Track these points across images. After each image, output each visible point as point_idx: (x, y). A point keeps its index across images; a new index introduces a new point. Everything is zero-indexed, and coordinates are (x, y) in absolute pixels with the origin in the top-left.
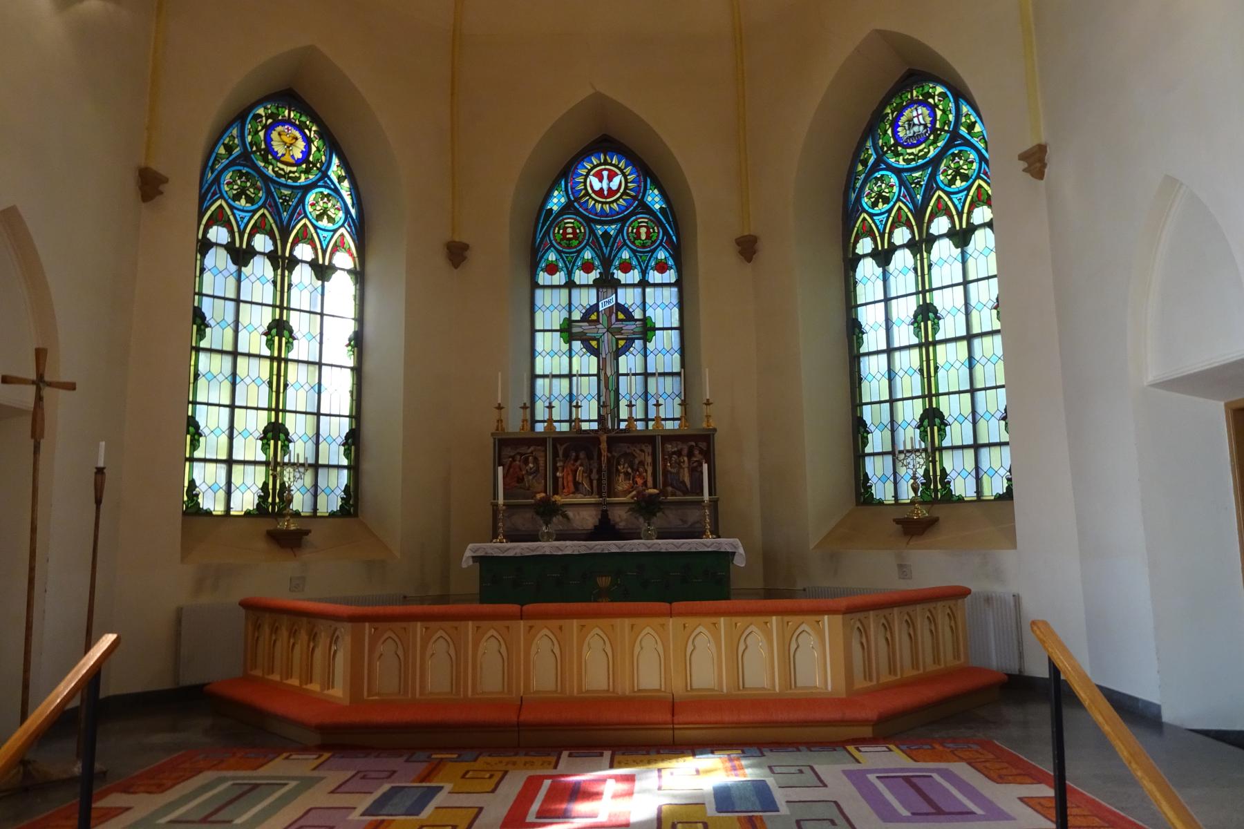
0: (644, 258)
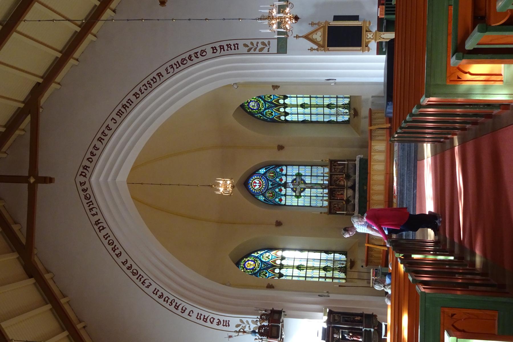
0: (279, 175)
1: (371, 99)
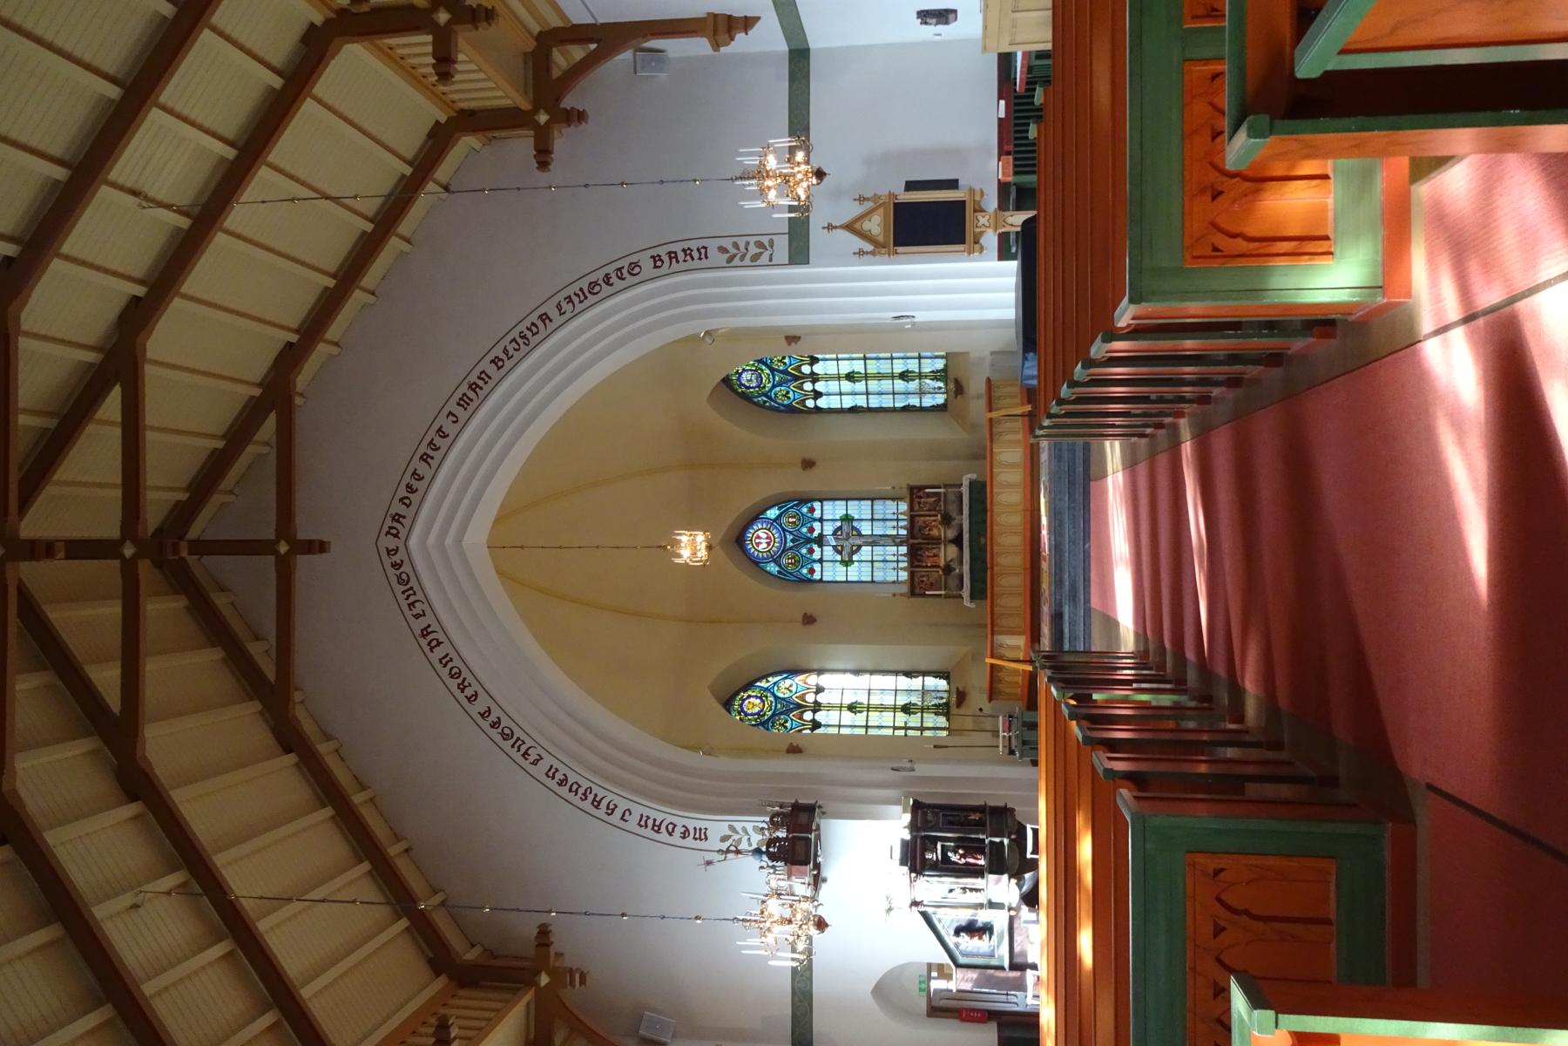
1: (988, 359)
